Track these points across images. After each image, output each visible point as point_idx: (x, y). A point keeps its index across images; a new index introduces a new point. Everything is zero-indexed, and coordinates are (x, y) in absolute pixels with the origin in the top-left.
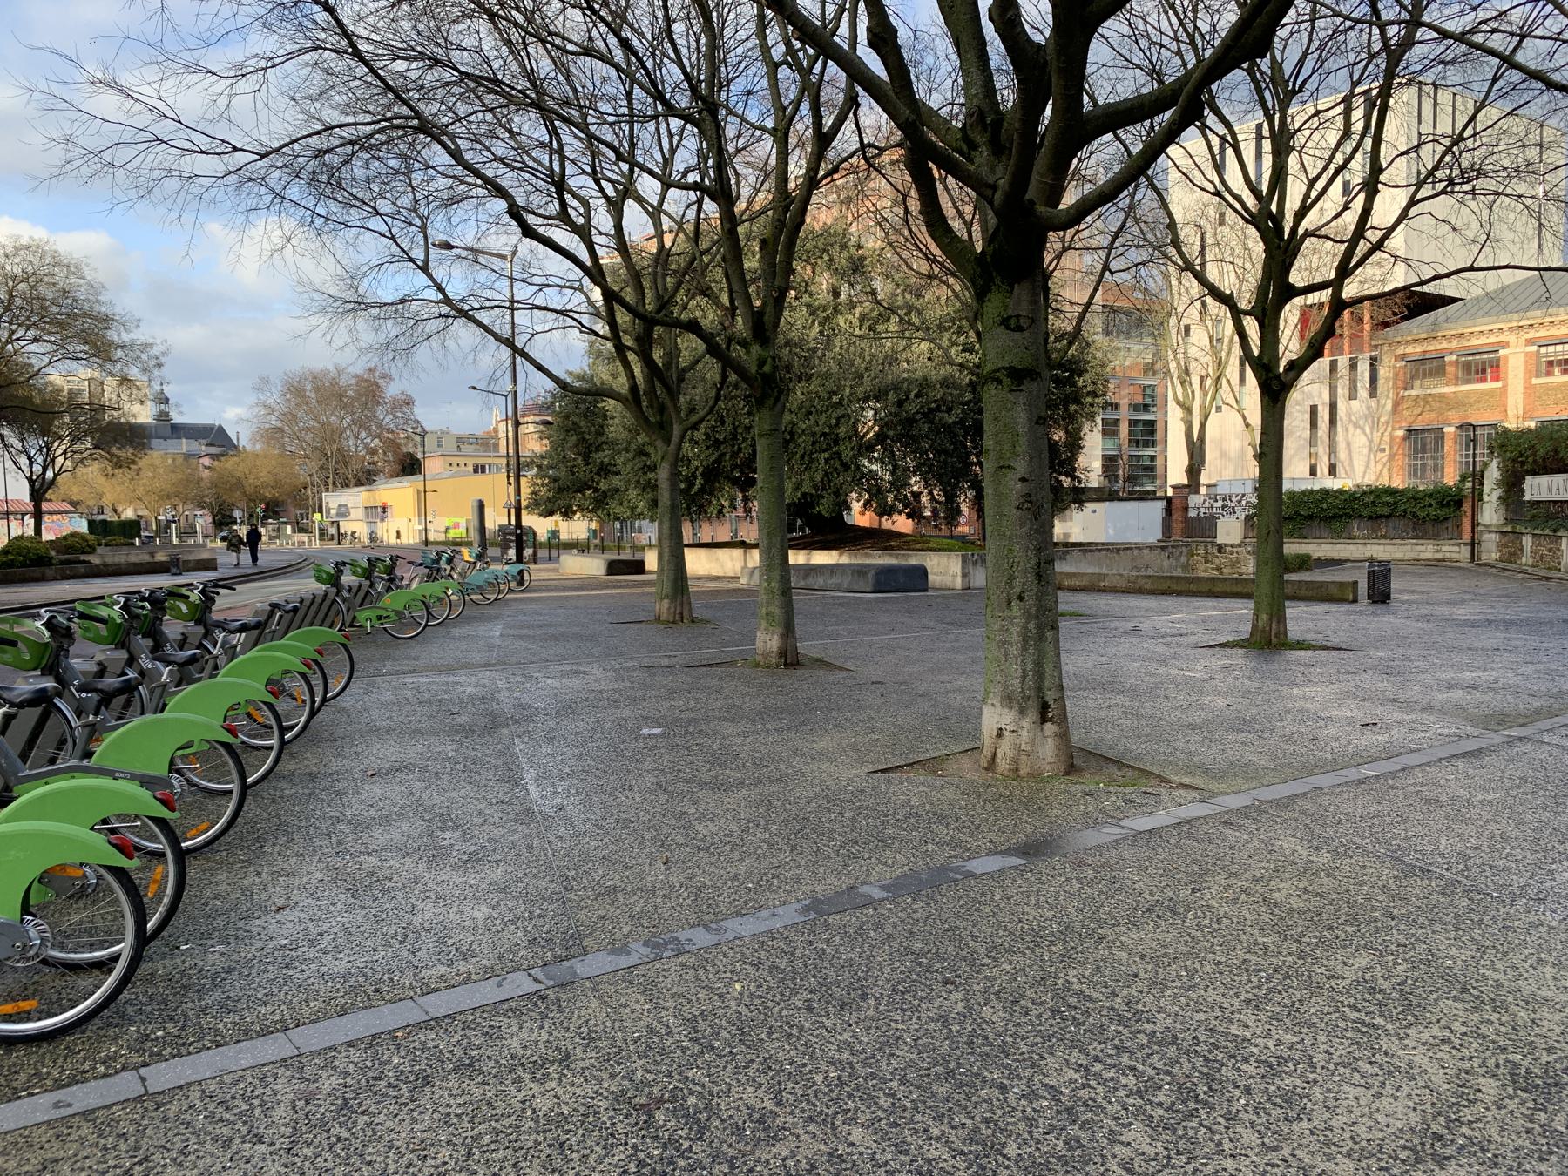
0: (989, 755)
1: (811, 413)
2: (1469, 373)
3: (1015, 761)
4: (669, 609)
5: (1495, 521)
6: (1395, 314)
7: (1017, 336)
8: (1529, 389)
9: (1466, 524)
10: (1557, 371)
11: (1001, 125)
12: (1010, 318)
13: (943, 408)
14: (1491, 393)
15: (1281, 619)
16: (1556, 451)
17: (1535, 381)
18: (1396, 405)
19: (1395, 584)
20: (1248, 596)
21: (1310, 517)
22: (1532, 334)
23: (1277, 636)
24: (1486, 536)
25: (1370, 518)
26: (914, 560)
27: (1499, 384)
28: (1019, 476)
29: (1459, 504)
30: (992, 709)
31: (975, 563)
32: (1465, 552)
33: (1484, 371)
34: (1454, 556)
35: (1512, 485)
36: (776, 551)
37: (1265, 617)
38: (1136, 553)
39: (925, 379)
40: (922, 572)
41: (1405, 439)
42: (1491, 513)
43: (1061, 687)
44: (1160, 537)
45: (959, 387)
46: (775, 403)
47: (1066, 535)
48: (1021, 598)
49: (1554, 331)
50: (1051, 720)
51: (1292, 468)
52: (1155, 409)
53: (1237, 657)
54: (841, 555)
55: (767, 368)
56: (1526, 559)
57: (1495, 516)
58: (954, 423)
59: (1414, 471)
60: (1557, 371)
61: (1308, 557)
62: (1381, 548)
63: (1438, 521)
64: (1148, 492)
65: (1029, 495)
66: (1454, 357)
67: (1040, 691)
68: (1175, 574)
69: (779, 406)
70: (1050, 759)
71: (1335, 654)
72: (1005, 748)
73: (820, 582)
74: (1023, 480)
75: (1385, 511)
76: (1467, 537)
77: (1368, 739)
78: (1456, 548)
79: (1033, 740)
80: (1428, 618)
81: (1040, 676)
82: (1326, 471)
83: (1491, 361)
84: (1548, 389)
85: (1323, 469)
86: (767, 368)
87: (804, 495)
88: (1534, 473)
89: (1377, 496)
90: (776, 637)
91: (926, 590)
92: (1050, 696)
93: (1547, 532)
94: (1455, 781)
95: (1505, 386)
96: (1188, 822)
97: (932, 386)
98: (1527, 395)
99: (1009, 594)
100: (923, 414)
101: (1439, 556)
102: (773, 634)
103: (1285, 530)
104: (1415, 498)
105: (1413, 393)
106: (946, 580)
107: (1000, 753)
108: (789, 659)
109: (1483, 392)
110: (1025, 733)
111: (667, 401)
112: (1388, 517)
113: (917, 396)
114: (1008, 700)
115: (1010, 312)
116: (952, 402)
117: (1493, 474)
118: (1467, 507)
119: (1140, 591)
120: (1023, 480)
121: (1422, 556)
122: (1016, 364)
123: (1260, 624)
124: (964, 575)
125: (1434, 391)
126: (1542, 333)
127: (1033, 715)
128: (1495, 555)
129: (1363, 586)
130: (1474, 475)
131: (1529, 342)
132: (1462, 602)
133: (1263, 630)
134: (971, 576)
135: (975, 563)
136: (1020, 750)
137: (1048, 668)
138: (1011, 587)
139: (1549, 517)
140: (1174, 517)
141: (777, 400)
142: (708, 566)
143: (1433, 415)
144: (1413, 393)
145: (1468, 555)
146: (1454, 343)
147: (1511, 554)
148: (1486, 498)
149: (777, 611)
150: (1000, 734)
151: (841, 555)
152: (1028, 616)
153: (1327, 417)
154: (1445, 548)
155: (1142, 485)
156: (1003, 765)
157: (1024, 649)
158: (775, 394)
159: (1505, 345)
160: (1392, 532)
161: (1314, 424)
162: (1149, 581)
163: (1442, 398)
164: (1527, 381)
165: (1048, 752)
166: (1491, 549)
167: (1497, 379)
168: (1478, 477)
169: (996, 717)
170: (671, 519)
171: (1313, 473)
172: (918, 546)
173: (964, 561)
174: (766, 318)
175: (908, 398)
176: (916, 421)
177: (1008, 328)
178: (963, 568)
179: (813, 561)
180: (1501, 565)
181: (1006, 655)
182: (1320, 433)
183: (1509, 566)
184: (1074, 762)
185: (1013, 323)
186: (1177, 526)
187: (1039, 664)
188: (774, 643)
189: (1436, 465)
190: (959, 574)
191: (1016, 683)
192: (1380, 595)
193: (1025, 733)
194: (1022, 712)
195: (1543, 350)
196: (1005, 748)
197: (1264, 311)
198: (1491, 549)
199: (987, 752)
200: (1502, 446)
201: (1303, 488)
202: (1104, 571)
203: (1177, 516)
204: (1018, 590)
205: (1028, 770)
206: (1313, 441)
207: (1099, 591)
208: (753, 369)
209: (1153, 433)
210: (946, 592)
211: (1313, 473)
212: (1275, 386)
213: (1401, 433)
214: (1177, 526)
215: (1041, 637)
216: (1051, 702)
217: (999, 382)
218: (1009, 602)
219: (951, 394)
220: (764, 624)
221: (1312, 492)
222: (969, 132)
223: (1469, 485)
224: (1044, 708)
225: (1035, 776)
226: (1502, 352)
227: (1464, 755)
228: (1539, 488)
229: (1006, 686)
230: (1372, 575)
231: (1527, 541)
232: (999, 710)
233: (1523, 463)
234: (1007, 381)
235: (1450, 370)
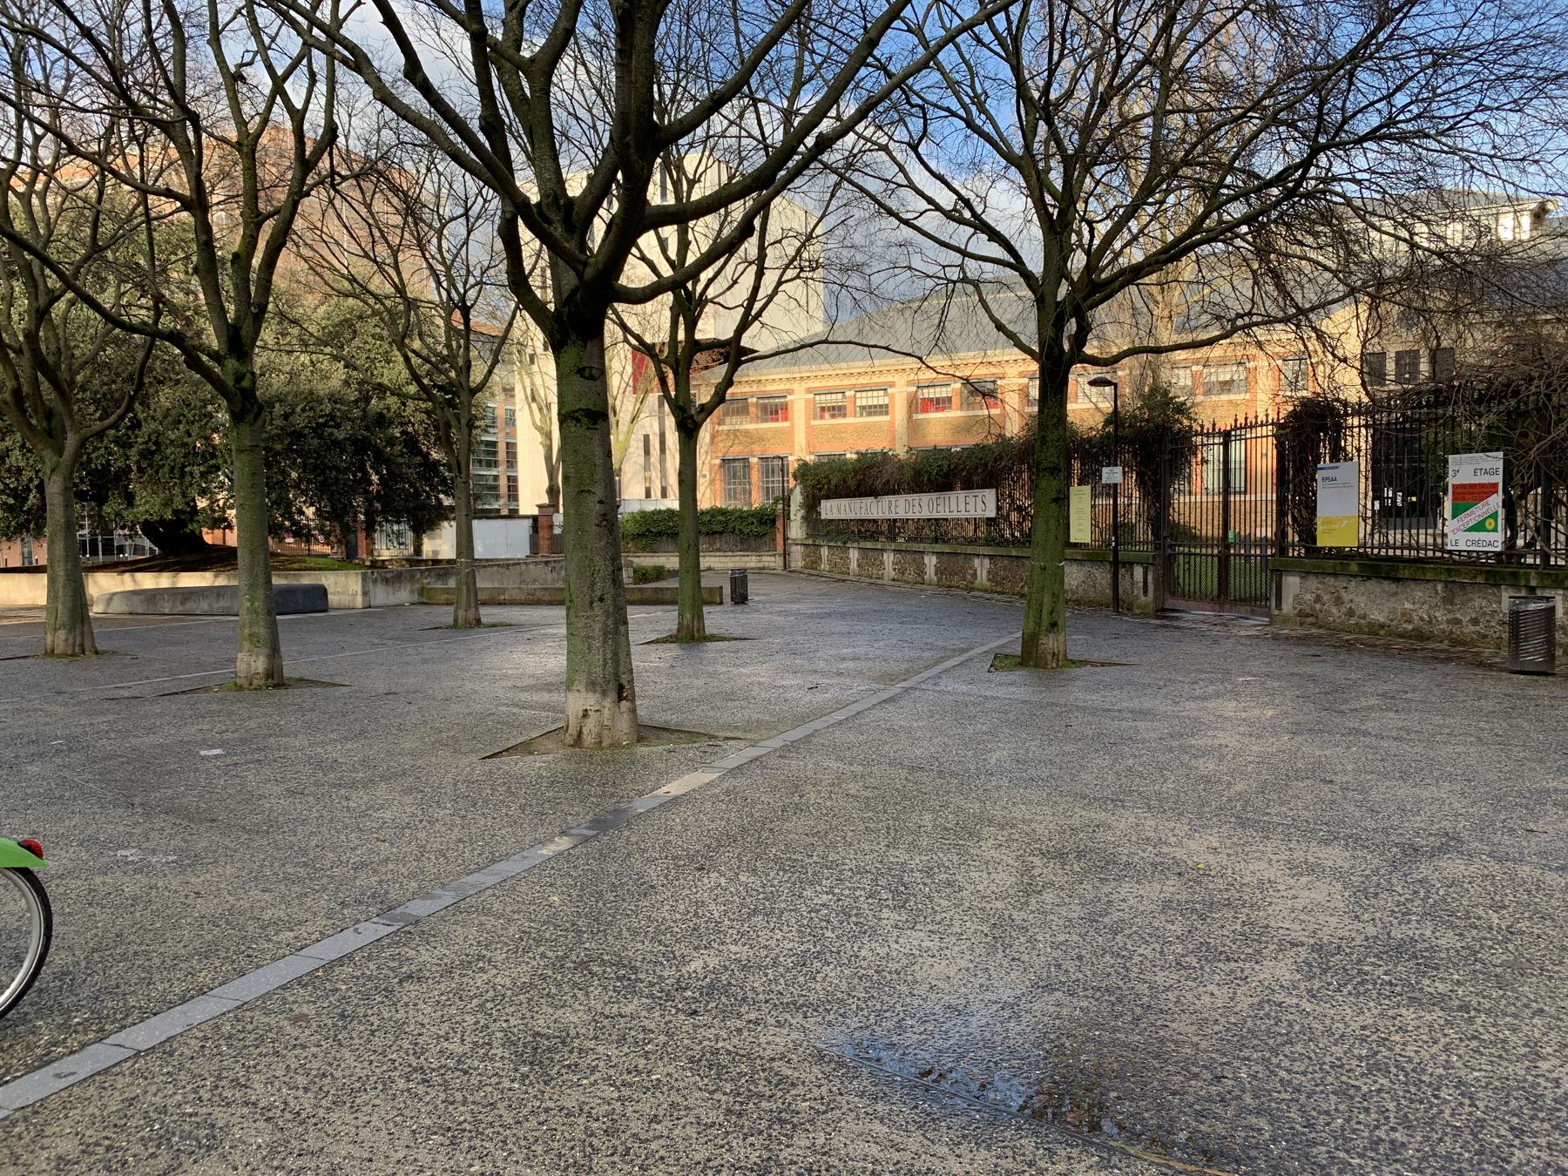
0: (575, 733)
1: (180, 422)
2: (766, 413)
3: (599, 735)
4: (66, 640)
5: (799, 536)
6: (714, 361)
7: (590, 383)
8: (809, 429)
9: (779, 538)
10: (827, 415)
11: (572, 209)
12: (584, 368)
13: (331, 423)
14: (781, 431)
15: (700, 618)
16: (845, 481)
17: (813, 423)
18: (713, 437)
19: (752, 588)
20: (561, 603)
21: (660, 534)
22: (810, 384)
23: (698, 631)
24: (794, 548)
25: (708, 534)
26: (307, 580)
27: (787, 424)
28: (597, 499)
29: (774, 522)
30: (578, 695)
31: (375, 581)
32: (779, 561)
33: (777, 413)
34: (772, 564)
35: (811, 505)
36: (259, 570)
37: (688, 616)
38: (523, 567)
39: (311, 393)
40: (322, 592)
41: (720, 467)
42: (796, 530)
43: (631, 671)
44: (528, 552)
45: (348, 403)
46: (256, 419)
47: (436, 552)
48: (601, 600)
49: (824, 383)
50: (625, 698)
51: (630, 490)
52: (496, 430)
53: (673, 650)
54: (216, 576)
55: (246, 383)
56: (824, 566)
57: (800, 532)
58: (345, 439)
59: (730, 494)
60: (827, 415)
61: (662, 567)
62: (717, 559)
63: (760, 536)
64: (490, 511)
65: (605, 515)
66: (755, 400)
67: (617, 675)
68: (557, 586)
69: (260, 422)
70: (625, 731)
71: (745, 642)
72: (590, 726)
73: (204, 606)
74: (601, 502)
75: (719, 528)
76: (780, 549)
77: (819, 698)
78: (773, 559)
79: (613, 716)
80: (786, 614)
81: (617, 662)
82: (659, 494)
83: (782, 404)
84: (823, 429)
85: (656, 492)
86: (246, 383)
87: (175, 512)
88: (828, 497)
89: (713, 516)
90: (262, 658)
91: (325, 611)
92: (624, 679)
93: (839, 544)
94: (895, 716)
95: (792, 426)
96: (757, 759)
97: (320, 401)
98: (808, 434)
99: (591, 597)
100: (312, 428)
101: (761, 565)
102: (257, 655)
103: (703, 547)
104: (741, 517)
105: (725, 428)
106: (345, 600)
107: (585, 731)
108: (275, 679)
109: (776, 430)
110: (606, 711)
111: (59, 407)
112: (721, 533)
113: (303, 410)
114: (592, 686)
115: (585, 364)
116: (342, 418)
117: (797, 499)
118: (779, 524)
119: (538, 603)
120: (601, 502)
121: (748, 565)
122: (591, 407)
123: (685, 622)
124: (365, 594)
125: (742, 427)
126: (817, 384)
127: (613, 695)
128: (801, 564)
129: (727, 591)
130: (783, 499)
131: (809, 390)
132: (797, 601)
133: (688, 627)
134: (372, 594)
135: (375, 581)
136: (603, 726)
137: (622, 656)
138: (593, 591)
139: (839, 532)
140: (541, 534)
141: (257, 416)
142: (31, 595)
143: (741, 447)
144: (725, 428)
145: (781, 564)
146: (755, 388)
147: (813, 562)
148: (792, 517)
149: (262, 631)
150: (585, 714)
151: (216, 576)
152: (607, 614)
153: (657, 446)
154: (764, 559)
155: (490, 504)
156: (588, 739)
157: (605, 642)
158: (256, 410)
159: (791, 392)
160: (725, 547)
161: (647, 452)
162: (547, 593)
163: (747, 433)
164: (808, 422)
165: (623, 725)
166: (797, 558)
167: (786, 419)
168: (786, 501)
169: (582, 701)
170: (66, 539)
171: (648, 495)
172: (296, 566)
173: (364, 580)
174: (243, 333)
175: (294, 411)
176: (304, 436)
177: (582, 376)
178: (363, 587)
179: (180, 585)
180: (807, 571)
181: (589, 648)
182: (652, 460)
183: (813, 572)
184: (645, 732)
185: (587, 373)
186: (544, 543)
187: (615, 654)
188: (260, 664)
189: (745, 489)
190: (360, 592)
191: (598, 671)
192: (740, 598)
193: (606, 711)
194: (604, 694)
195: (818, 397)
196: (590, 726)
197: (677, 361)
198: (797, 561)
199: (573, 731)
200: (803, 475)
201: (652, 508)
202: (496, 585)
203: (542, 533)
204: (599, 593)
205: (610, 741)
206: (647, 467)
207: (500, 604)
208: (230, 383)
209: (495, 453)
210: (342, 612)
211: (648, 495)
212: (690, 424)
213: (718, 462)
214: (544, 543)
215: (616, 631)
216: (626, 684)
217: (578, 420)
218: (592, 603)
219: (339, 410)
220: (247, 645)
221: (660, 512)
222: (544, 209)
223: (780, 506)
224: (621, 688)
225: (615, 745)
226: (789, 397)
227: (885, 701)
228: (831, 509)
229: (590, 674)
230: (734, 581)
231: (825, 552)
232: (584, 694)
233: (820, 490)
234: (585, 420)
235: (752, 410)
